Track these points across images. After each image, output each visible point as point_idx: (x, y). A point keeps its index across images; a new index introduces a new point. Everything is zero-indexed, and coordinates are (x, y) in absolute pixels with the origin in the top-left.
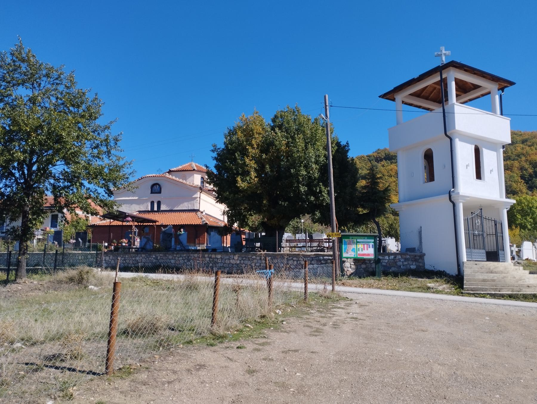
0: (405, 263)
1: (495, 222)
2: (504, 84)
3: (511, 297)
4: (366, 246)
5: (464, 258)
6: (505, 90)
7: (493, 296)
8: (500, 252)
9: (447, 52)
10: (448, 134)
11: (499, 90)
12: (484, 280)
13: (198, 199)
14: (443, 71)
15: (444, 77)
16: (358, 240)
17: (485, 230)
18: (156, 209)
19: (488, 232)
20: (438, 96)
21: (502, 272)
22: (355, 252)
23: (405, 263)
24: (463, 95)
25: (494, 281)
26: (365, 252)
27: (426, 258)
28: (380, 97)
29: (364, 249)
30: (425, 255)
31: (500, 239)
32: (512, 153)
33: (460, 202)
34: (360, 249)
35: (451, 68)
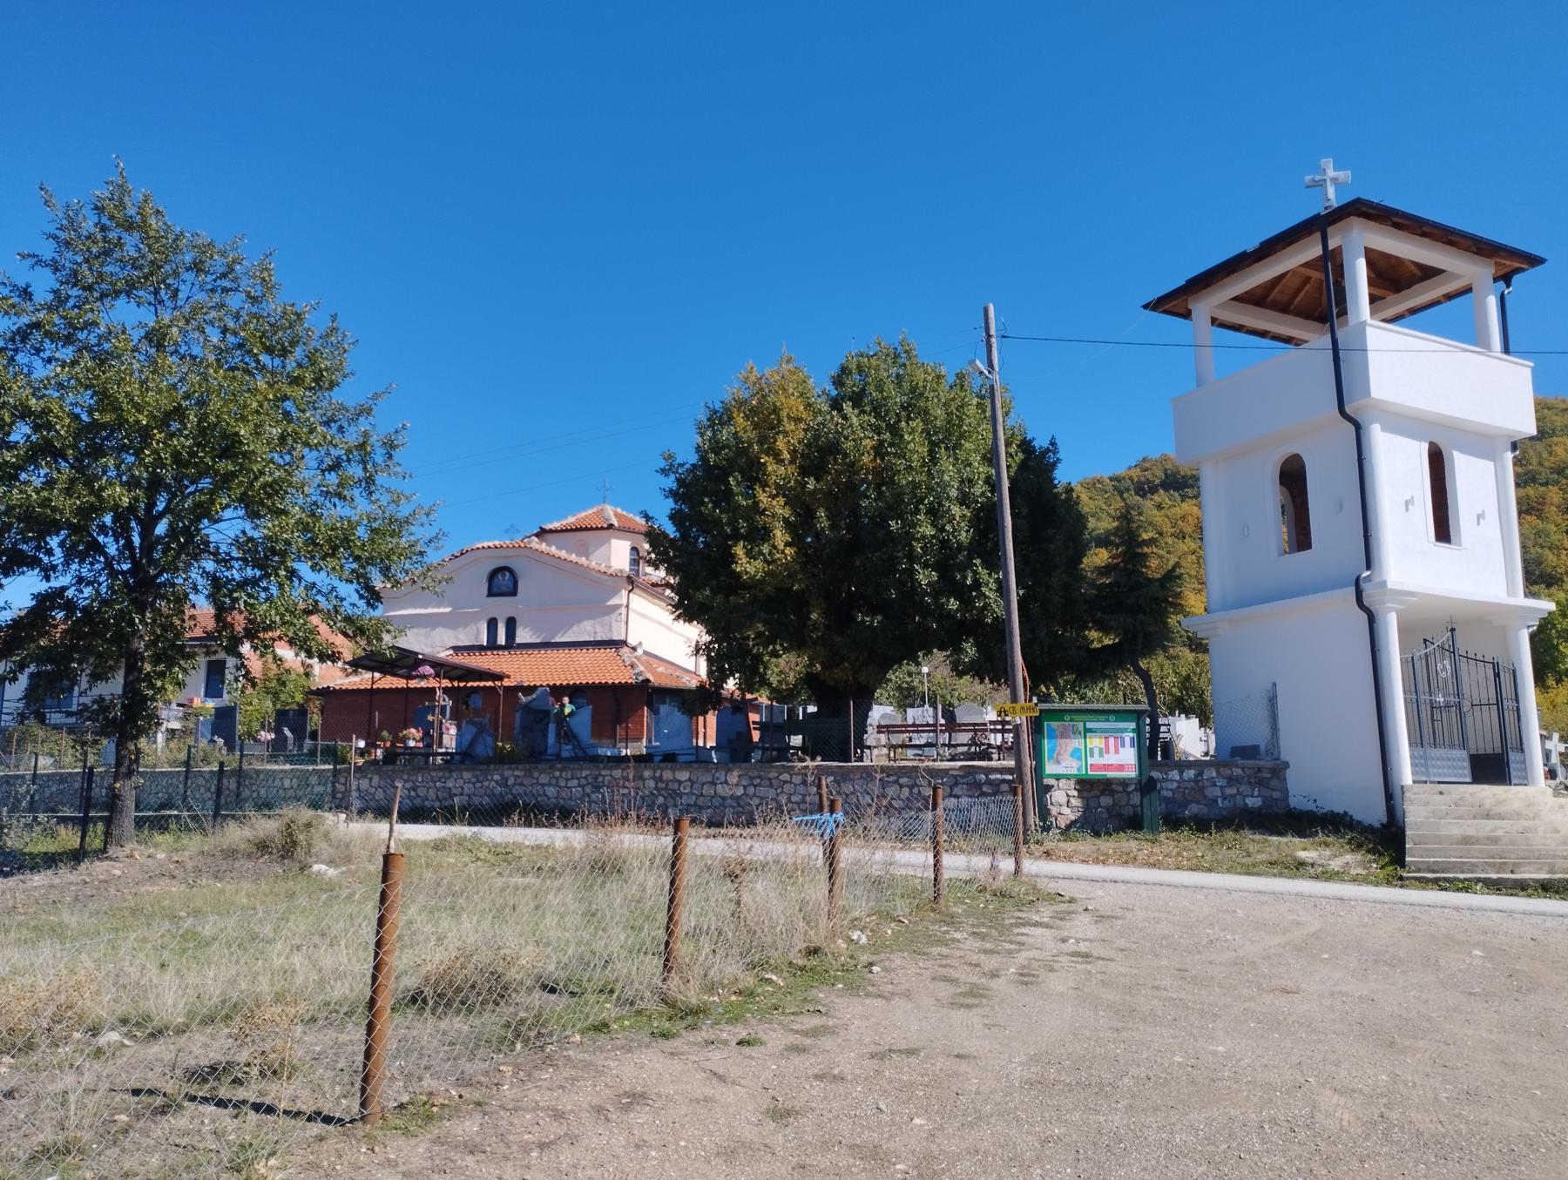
0: (1229, 791)
1: (1496, 667)
2: (1510, 262)
4: (1112, 741)
5: (1406, 773)
6: (1516, 279)
7: (1495, 886)
8: (1513, 756)
9: (1341, 175)
10: (1348, 410)
11: (1496, 280)
12: (1466, 840)
13: (623, 610)
15: (1332, 245)
16: (1089, 725)
18: (502, 640)
19: (1475, 696)
20: (1319, 302)
22: (1079, 759)
23: (1229, 791)
24: (1391, 298)
26: (1111, 759)
27: (1291, 776)
28: (1145, 307)
29: (1107, 752)
30: (1286, 765)
31: (1510, 717)
32: (1540, 464)
33: (1391, 610)
34: (1096, 752)
35: (1353, 218)
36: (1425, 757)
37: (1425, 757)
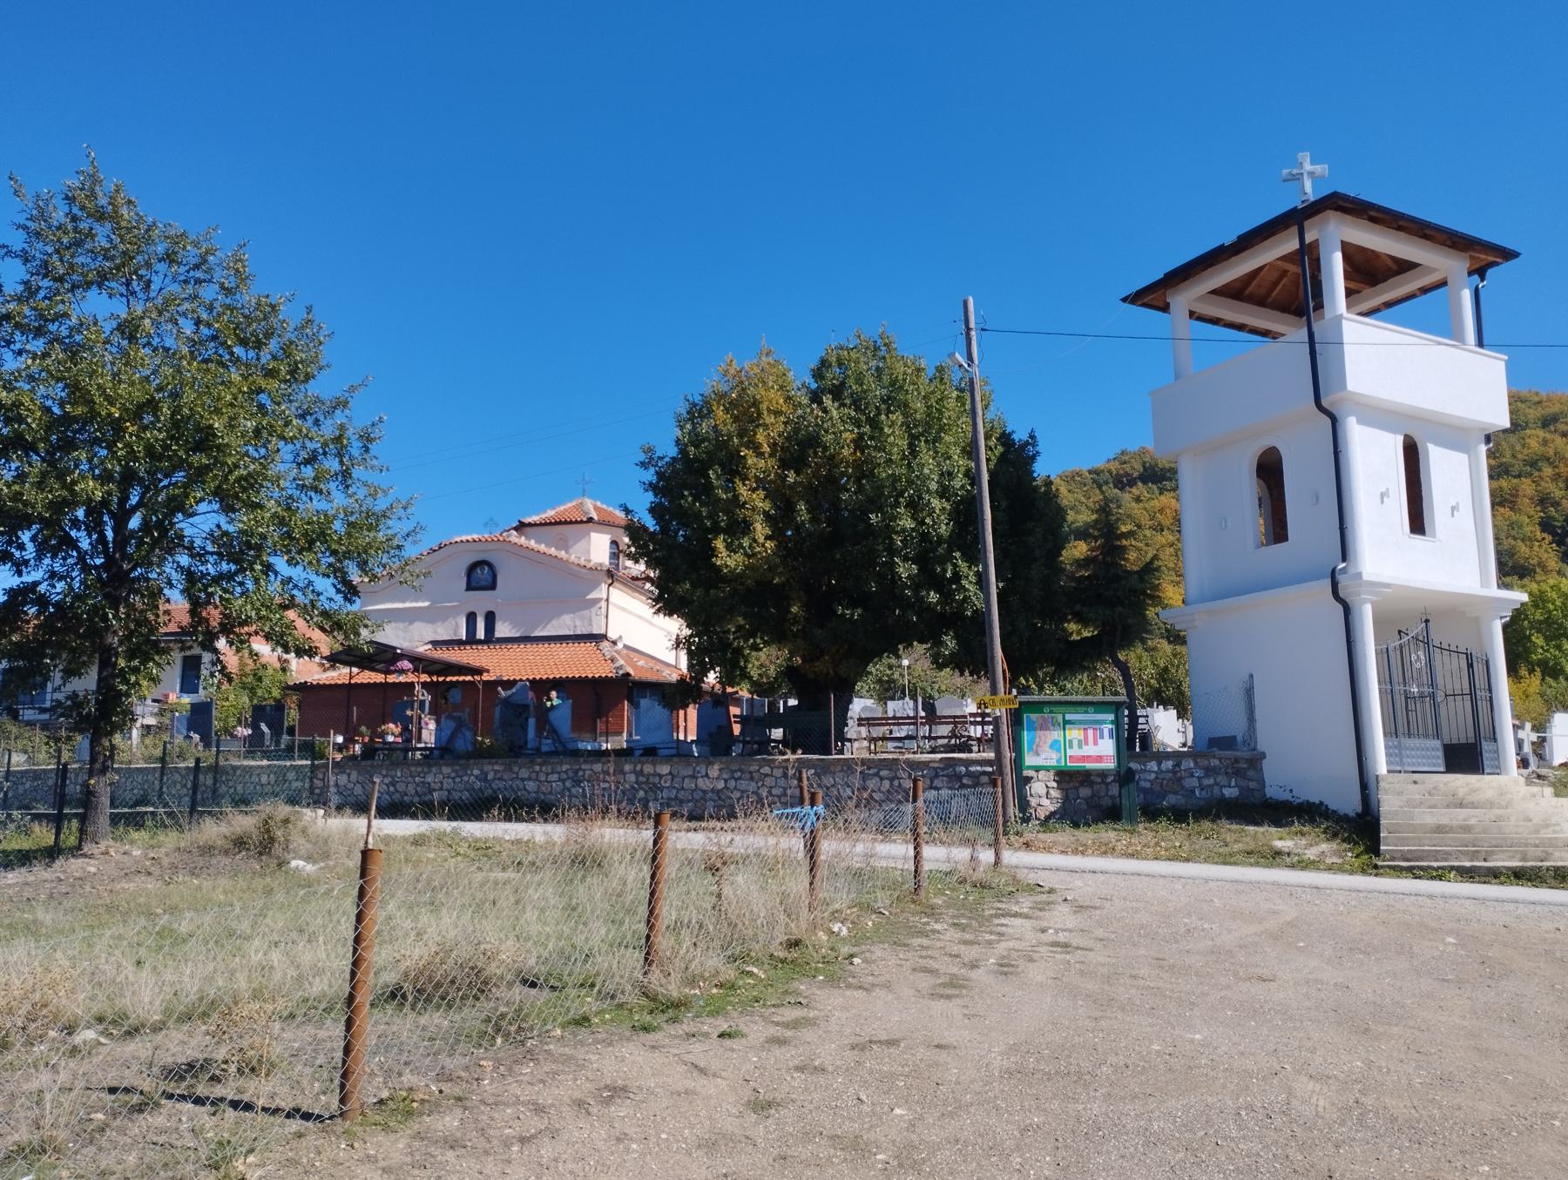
0: (1206, 782)
1: (1469, 658)
2: (1485, 256)
3: (1519, 876)
4: (1090, 732)
5: (1380, 763)
6: (1490, 273)
7: (1468, 874)
8: (1486, 746)
9: (1319, 169)
10: (1324, 403)
11: (1470, 273)
12: (1440, 829)
14: (1306, 223)
15: (1309, 239)
16: (1068, 717)
17: (1440, 680)
19: (1449, 687)
20: (1294, 295)
21: (1490, 804)
22: (1059, 751)
23: (1206, 782)
24: (1368, 291)
25: (1467, 829)
26: (1090, 750)
27: (1266, 764)
28: (1124, 300)
29: (1087, 743)
30: (1263, 756)
31: (1483, 707)
32: (1514, 456)
33: (1366, 601)
34: (1075, 743)
35: (1330, 213)
36: (1399, 747)
37: (1399, 747)
